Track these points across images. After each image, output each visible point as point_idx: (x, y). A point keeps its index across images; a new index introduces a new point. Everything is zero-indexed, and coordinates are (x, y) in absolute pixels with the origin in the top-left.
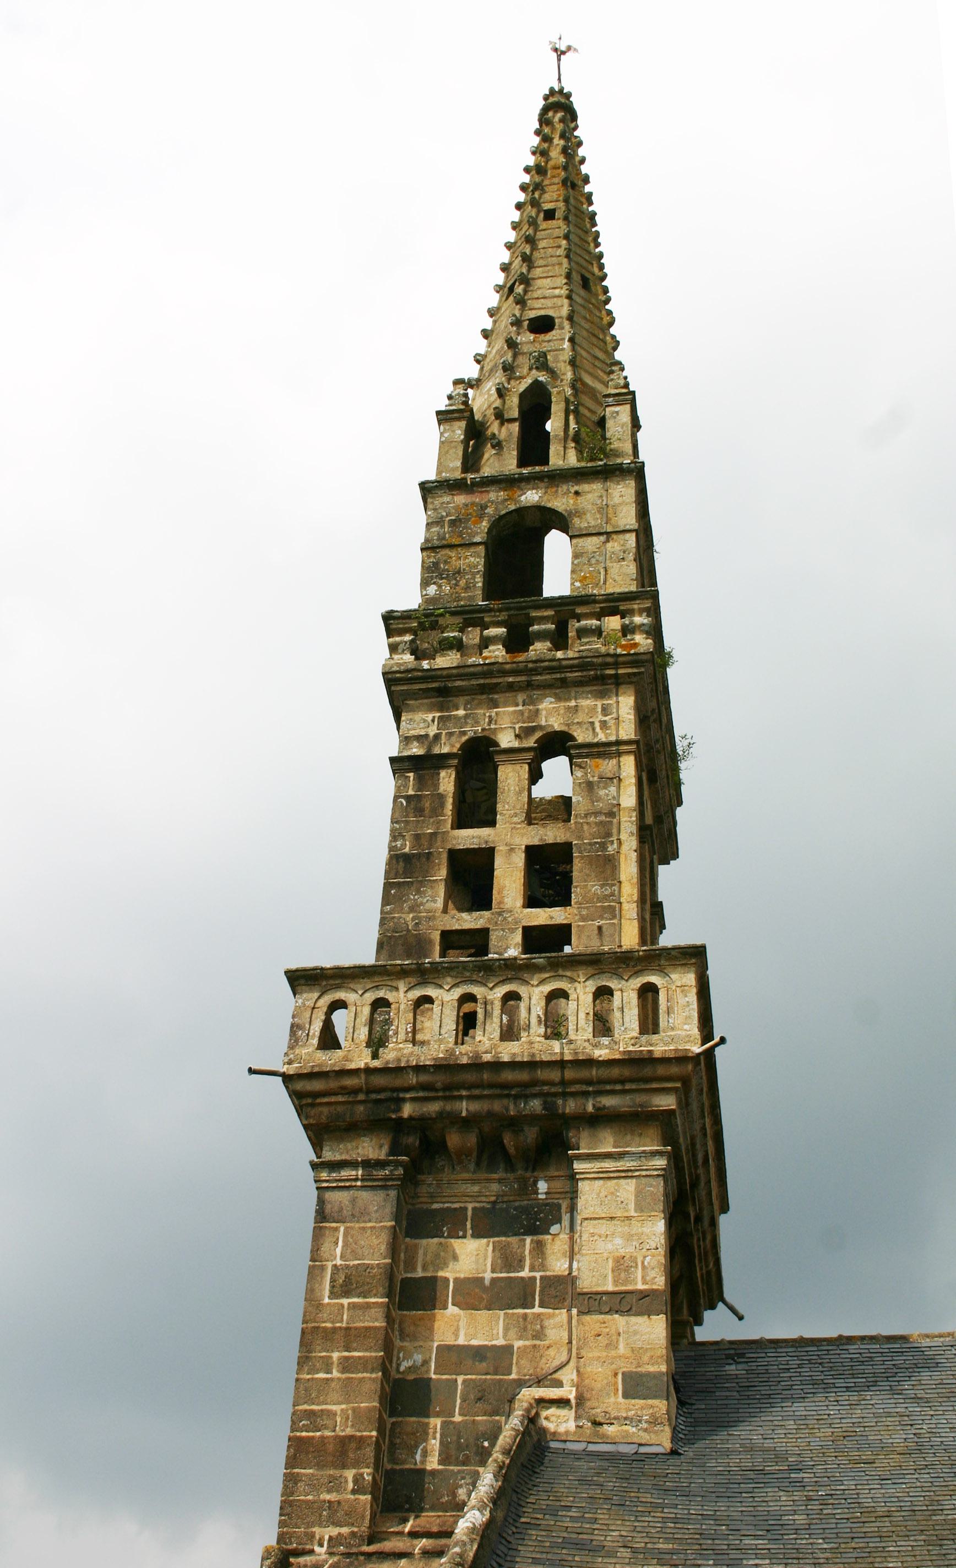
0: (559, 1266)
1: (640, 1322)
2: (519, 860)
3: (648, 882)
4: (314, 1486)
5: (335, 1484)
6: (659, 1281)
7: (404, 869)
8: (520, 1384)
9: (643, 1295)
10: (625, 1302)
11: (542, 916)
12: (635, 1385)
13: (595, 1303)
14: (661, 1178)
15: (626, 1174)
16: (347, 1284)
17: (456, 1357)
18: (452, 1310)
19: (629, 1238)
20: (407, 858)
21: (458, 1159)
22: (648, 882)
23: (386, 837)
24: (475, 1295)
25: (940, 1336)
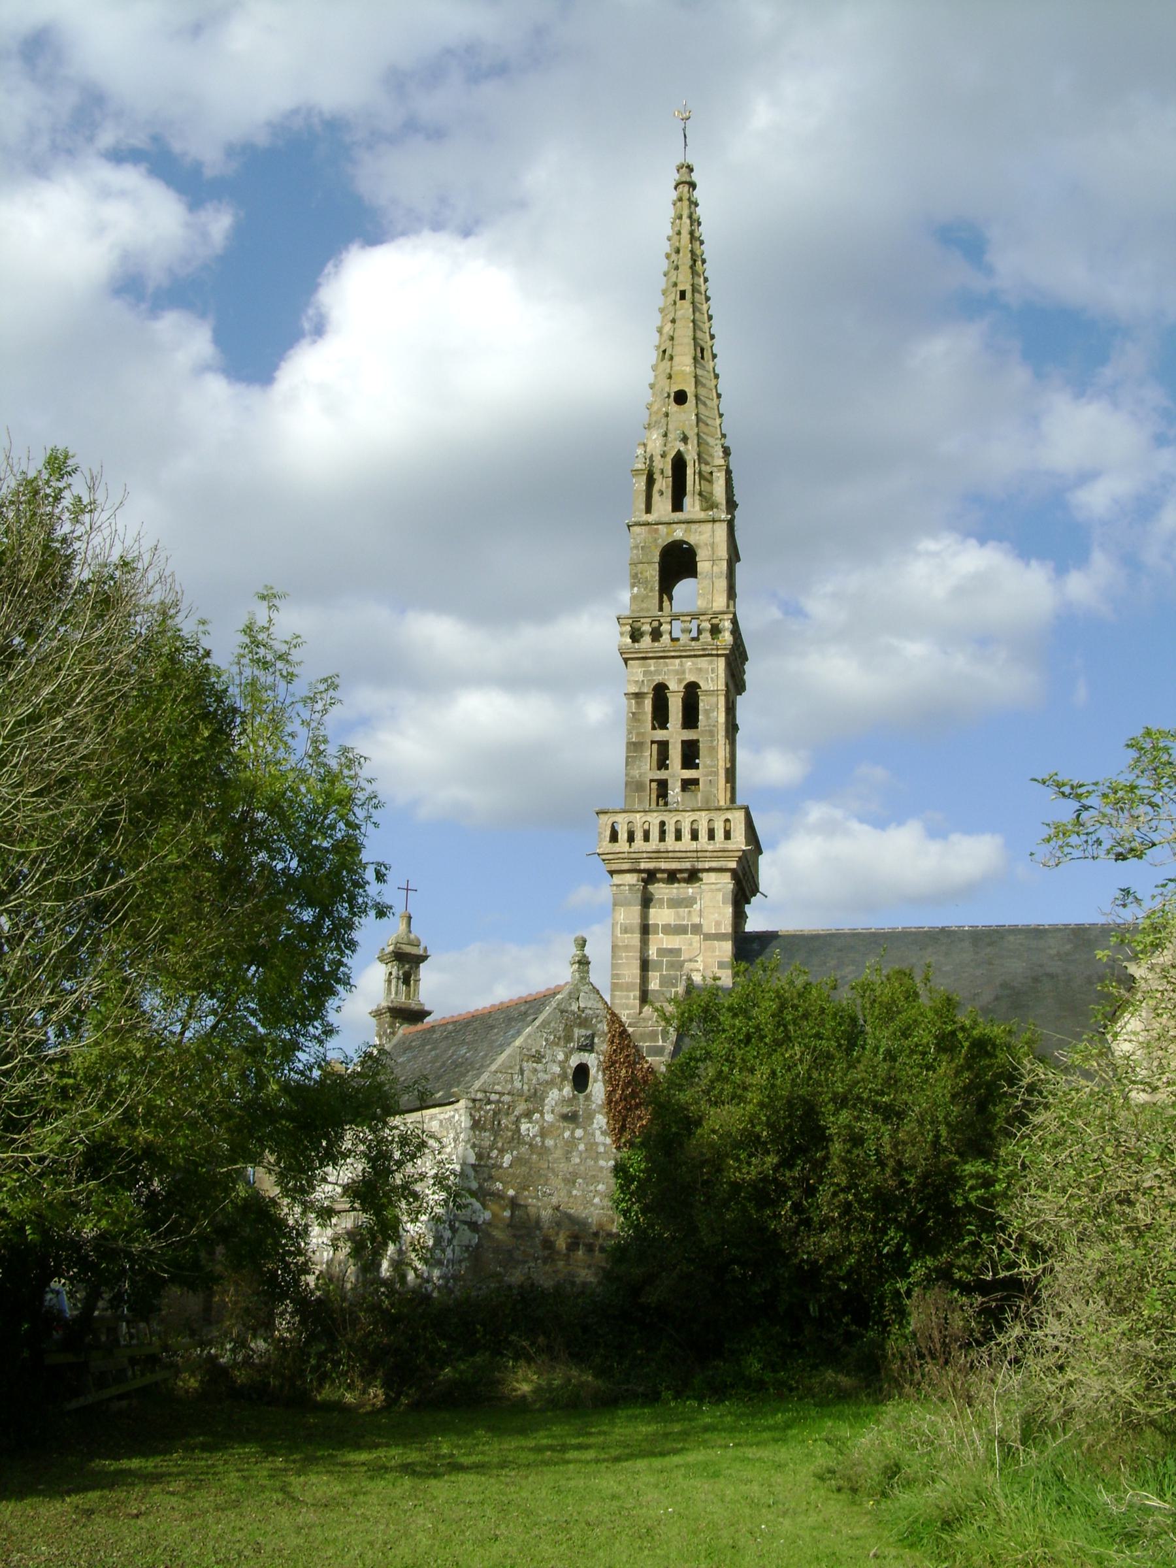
0: (696, 920)
1: (723, 943)
2: (679, 746)
3: (731, 710)
4: (621, 998)
5: (628, 998)
6: (730, 930)
7: (634, 747)
8: (685, 961)
9: (724, 934)
10: (718, 937)
11: (689, 774)
12: (721, 965)
13: (708, 937)
14: (729, 875)
15: (719, 890)
16: (625, 930)
17: (662, 952)
18: (661, 935)
19: (719, 914)
20: (634, 744)
21: (658, 881)
22: (731, 710)
23: (625, 733)
24: (670, 930)
25: (732, 728)
